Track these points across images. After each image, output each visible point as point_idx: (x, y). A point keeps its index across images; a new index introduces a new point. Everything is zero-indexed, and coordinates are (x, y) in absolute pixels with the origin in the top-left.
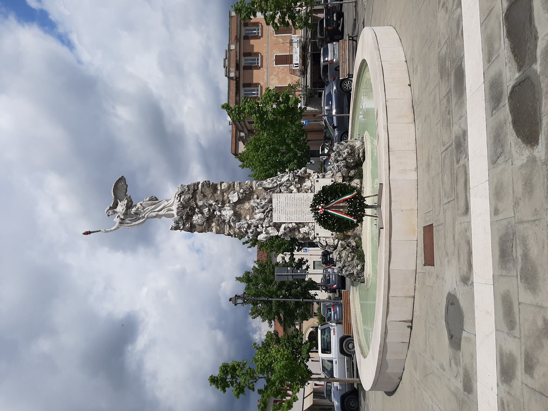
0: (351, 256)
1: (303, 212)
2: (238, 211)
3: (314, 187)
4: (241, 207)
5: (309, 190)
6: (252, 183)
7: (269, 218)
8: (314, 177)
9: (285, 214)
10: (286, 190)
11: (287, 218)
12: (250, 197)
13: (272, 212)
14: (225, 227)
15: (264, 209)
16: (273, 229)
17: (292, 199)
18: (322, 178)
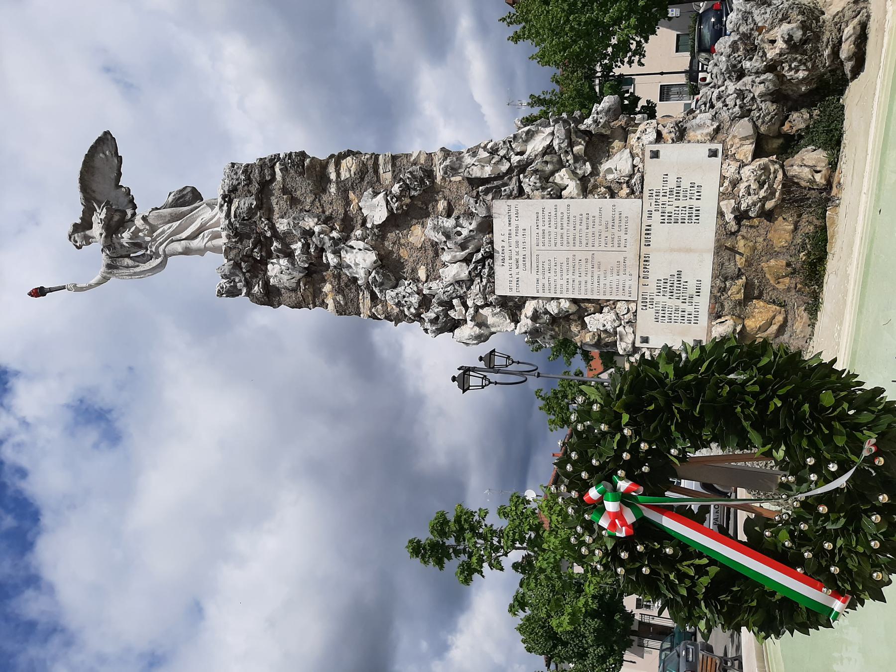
1: (596, 266)
2: (392, 252)
3: (643, 177)
6: (432, 160)
7: (485, 281)
8: (644, 137)
9: (534, 272)
11: (540, 285)
12: (427, 208)
13: (493, 263)
14: (360, 297)
17: (559, 220)
18: (673, 141)
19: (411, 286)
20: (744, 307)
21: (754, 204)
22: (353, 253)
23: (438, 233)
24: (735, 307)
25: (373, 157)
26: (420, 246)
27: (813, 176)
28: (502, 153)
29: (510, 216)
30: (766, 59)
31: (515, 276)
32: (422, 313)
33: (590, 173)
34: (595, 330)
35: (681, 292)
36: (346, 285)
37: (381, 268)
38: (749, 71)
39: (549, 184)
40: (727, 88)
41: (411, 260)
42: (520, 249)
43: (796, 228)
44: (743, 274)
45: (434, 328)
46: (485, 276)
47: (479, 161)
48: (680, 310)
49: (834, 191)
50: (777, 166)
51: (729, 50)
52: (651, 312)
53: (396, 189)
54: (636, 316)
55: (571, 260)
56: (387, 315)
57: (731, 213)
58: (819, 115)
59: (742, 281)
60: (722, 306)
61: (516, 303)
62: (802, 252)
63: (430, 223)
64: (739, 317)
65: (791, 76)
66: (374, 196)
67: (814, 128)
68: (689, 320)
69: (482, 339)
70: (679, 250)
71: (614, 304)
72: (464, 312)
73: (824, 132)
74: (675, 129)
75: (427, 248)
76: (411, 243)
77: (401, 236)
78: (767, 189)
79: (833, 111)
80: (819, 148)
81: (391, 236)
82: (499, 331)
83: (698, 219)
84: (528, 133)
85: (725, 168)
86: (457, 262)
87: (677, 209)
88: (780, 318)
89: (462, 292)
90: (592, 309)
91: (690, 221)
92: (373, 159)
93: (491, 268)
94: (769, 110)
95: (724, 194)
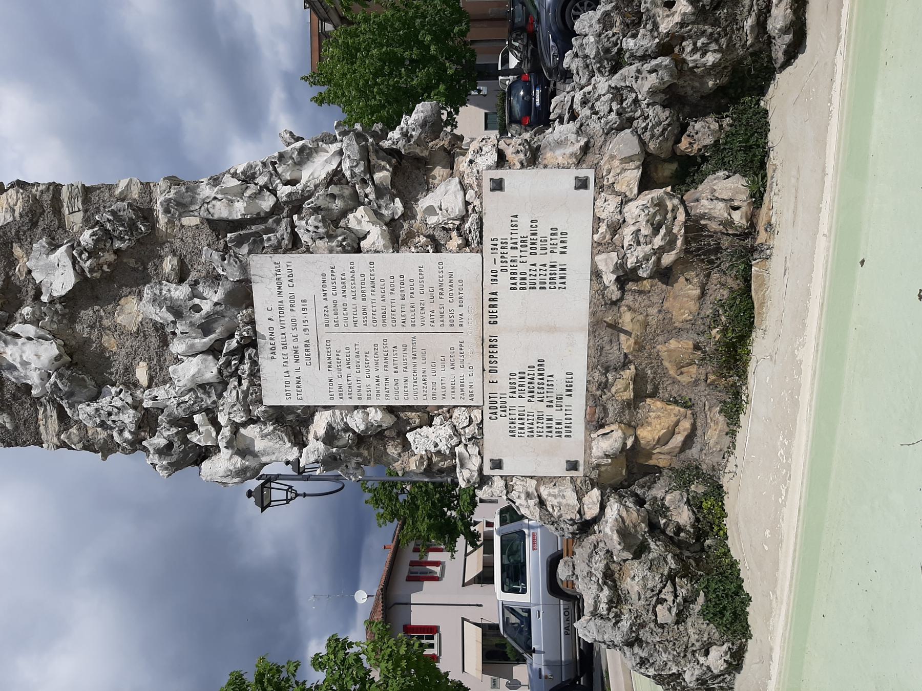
0: (676, 596)
1: (419, 356)
2: (88, 341)
3: (481, 219)
4: (101, 318)
5: (454, 233)
6: (151, 193)
7: (245, 383)
8: (479, 160)
9: (324, 366)
10: (327, 233)
11: (335, 387)
12: (145, 269)
13: (256, 354)
14: (40, 416)
15: (212, 336)
16: (269, 434)
17: (358, 285)
18: (523, 166)
19: (121, 396)
20: (635, 409)
21: (647, 258)
22: (16, 344)
23: (161, 308)
24: (622, 411)
25: (51, 188)
26: (135, 329)
27: (730, 215)
28: (262, 180)
29: (279, 279)
30: (659, 34)
31: (294, 375)
32: (144, 439)
33: (403, 215)
34: (424, 453)
35: (545, 391)
36: (14, 396)
37: (68, 368)
38: (632, 55)
39: (339, 231)
40: (595, 88)
41: (123, 352)
42: (300, 332)
43: (703, 294)
44: (630, 362)
45: (165, 463)
46: (245, 376)
47: (224, 192)
48: (545, 417)
49: (762, 237)
50: (676, 201)
51: (597, 27)
52: (503, 423)
53: (86, 238)
54: (482, 428)
55: (380, 347)
56: (86, 443)
57: (613, 272)
58: (731, 125)
59: (629, 373)
60: (605, 410)
61: (299, 416)
62: (715, 328)
63: (147, 291)
64: (629, 425)
65: (695, 61)
66: (52, 250)
67: (725, 144)
68: (559, 432)
69: (248, 475)
70: (539, 329)
71: (448, 411)
72: (214, 434)
73: (741, 150)
74: (524, 147)
75: (147, 333)
76: (120, 325)
77: (103, 314)
78: (665, 235)
79: (751, 118)
80: (735, 173)
81: (87, 314)
82: (274, 461)
83: (564, 283)
84: (302, 150)
85: (600, 205)
86: (197, 354)
87: (533, 268)
88: (686, 425)
89: (209, 402)
90: (417, 421)
91: (552, 286)
92: (51, 192)
93: (254, 363)
94: (659, 118)
95: (599, 244)
